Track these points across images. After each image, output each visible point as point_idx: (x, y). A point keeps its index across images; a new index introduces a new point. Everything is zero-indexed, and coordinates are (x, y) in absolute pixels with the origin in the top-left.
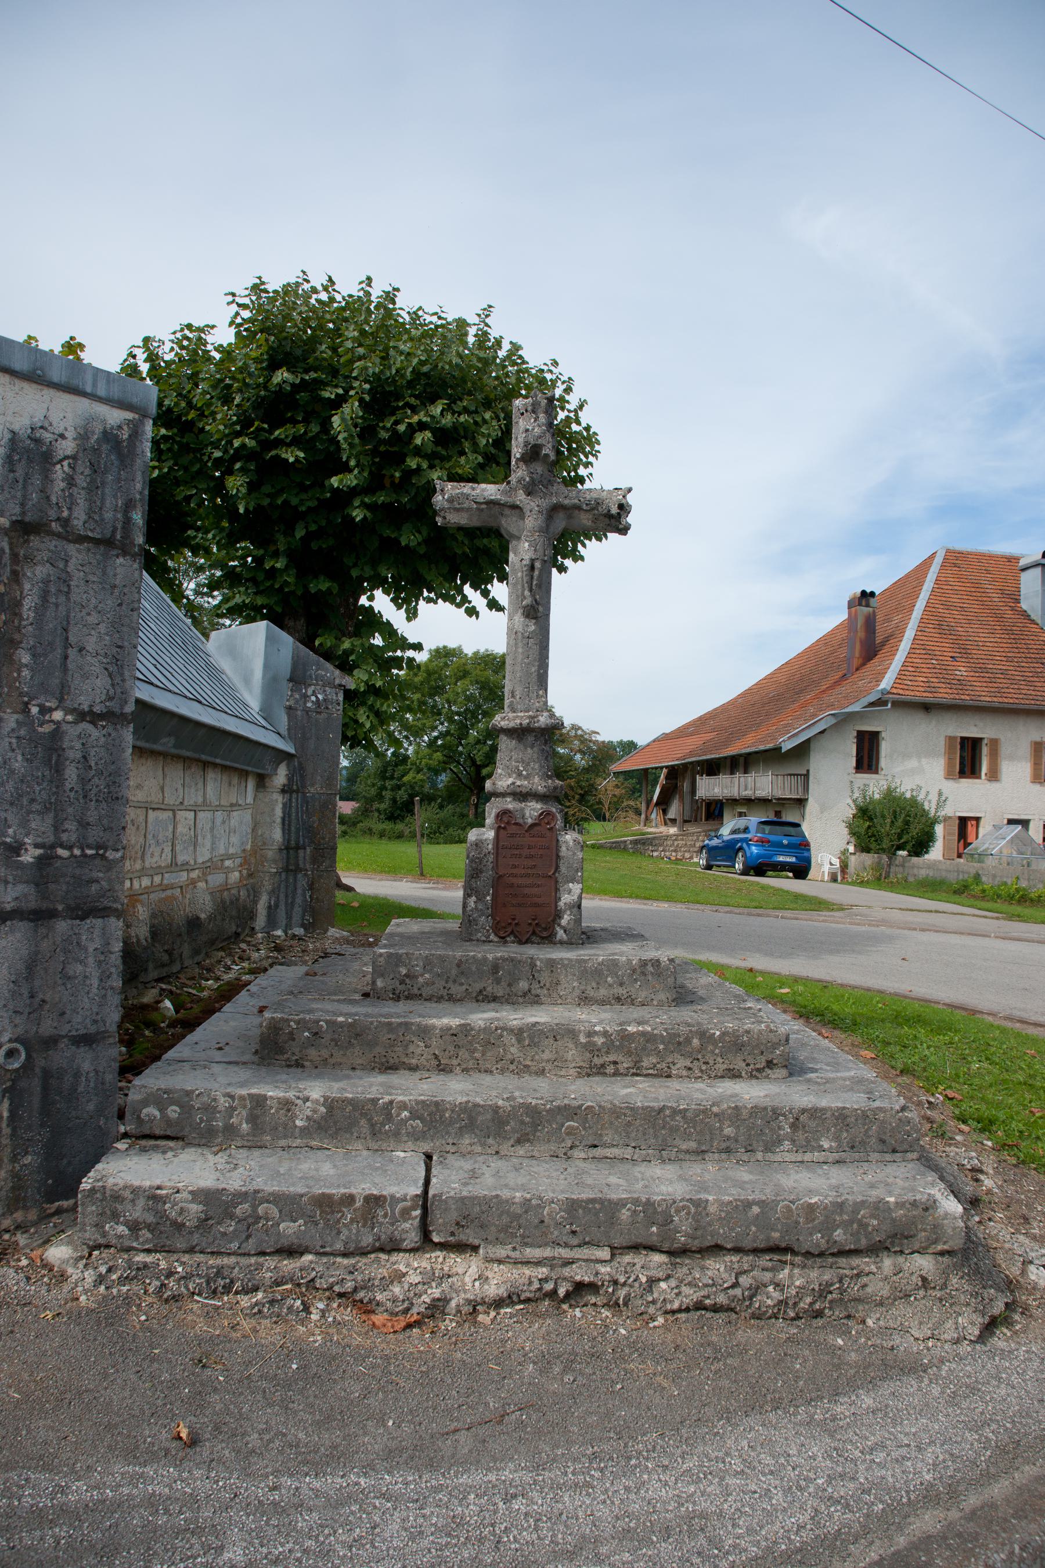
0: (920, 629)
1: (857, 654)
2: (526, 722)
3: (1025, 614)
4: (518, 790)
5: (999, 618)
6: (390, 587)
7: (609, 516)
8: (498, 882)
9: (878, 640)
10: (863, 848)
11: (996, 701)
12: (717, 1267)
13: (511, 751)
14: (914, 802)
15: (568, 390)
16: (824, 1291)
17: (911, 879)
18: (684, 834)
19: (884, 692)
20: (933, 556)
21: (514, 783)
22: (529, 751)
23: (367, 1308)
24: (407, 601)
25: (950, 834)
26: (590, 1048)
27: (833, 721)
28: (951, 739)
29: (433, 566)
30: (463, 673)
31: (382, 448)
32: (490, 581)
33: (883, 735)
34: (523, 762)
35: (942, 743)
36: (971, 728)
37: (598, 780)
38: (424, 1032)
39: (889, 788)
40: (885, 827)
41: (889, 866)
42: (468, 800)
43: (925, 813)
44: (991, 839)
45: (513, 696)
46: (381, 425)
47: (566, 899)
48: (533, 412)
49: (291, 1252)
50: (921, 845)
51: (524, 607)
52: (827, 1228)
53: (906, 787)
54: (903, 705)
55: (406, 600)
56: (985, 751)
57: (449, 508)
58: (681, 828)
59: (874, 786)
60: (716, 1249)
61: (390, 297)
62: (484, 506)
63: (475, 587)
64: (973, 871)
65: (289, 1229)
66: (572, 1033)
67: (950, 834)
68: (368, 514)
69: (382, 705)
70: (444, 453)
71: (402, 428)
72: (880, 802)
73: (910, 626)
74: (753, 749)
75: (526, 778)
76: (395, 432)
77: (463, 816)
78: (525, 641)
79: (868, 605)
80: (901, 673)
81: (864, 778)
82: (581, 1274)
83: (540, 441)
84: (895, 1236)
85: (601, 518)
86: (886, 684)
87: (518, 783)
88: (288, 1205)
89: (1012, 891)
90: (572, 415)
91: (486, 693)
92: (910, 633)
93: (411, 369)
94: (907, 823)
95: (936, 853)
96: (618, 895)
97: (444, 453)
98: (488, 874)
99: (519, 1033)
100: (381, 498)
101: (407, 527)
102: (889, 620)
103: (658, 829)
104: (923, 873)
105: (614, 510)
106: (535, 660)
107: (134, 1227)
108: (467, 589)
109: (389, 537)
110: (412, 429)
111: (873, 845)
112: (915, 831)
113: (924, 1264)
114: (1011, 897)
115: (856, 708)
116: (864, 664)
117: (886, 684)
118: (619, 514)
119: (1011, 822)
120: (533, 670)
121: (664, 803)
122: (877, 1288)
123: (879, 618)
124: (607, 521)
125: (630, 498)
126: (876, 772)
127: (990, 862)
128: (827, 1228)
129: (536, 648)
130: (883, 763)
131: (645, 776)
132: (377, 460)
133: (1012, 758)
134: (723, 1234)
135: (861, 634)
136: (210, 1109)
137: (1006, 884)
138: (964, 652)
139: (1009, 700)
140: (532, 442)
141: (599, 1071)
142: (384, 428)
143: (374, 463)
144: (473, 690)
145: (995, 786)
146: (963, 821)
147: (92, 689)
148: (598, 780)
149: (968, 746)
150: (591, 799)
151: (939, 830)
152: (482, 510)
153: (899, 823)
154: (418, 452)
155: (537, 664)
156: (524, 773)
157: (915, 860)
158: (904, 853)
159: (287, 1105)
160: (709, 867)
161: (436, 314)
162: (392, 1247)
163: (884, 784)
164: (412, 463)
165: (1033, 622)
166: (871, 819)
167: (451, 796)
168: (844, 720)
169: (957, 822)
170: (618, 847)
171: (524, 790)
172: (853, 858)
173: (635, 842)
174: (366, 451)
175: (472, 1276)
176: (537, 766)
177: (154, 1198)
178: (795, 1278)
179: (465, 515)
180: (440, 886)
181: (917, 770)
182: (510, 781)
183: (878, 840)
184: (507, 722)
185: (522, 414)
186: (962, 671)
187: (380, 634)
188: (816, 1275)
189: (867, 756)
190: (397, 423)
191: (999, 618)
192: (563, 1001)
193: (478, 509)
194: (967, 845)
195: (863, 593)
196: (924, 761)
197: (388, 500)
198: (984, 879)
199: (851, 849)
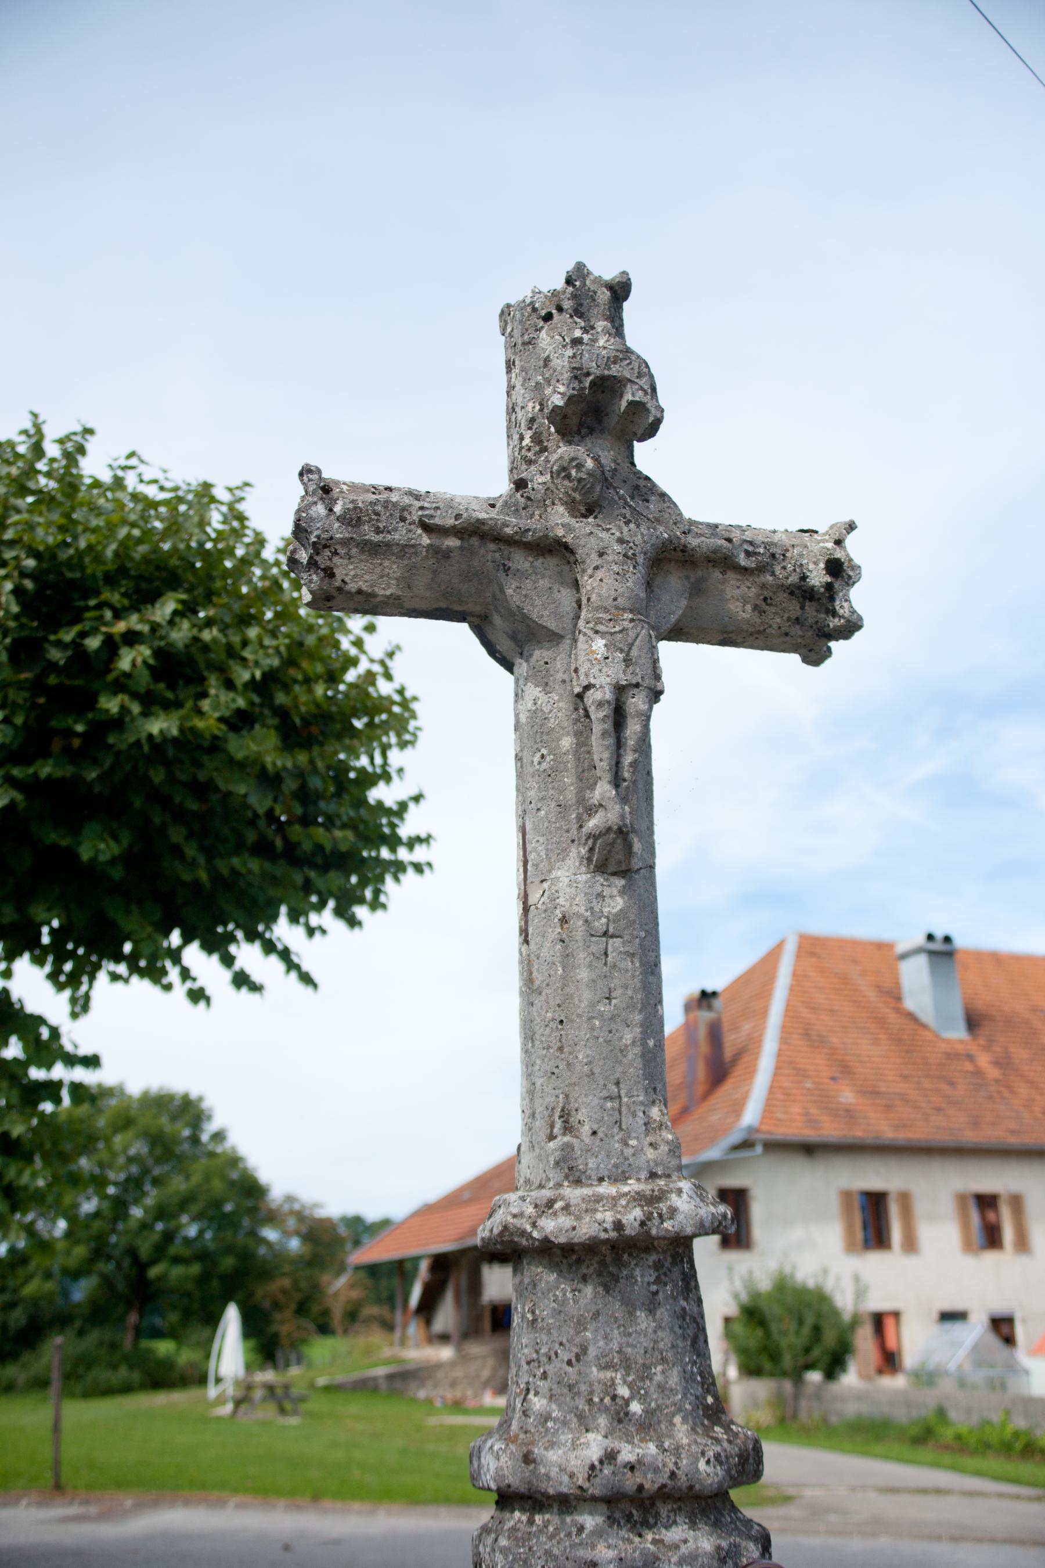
0: (785, 1038)
2: (633, 1216)
3: (911, 1017)
4: (630, 1482)
5: (881, 1022)
6: (45, 950)
7: (803, 592)
11: (901, 1136)
13: (581, 1325)
18: (463, 1358)
19: (750, 1130)
21: (610, 1456)
22: (643, 1321)
24: (73, 980)
28: (846, 1196)
29: (134, 908)
30: (125, 1121)
31: (52, 680)
32: (231, 938)
34: (627, 1364)
35: (834, 1204)
36: (874, 1176)
37: (325, 1278)
40: (790, 1339)
42: (122, 1319)
43: (835, 1313)
45: (568, 1129)
46: (52, 638)
48: (578, 312)
50: (834, 1365)
51: (594, 837)
53: (805, 1272)
54: (777, 1147)
55: (73, 980)
56: (894, 1211)
57: (346, 542)
58: (458, 1349)
61: (74, 450)
62: (452, 542)
63: (209, 947)
68: (19, 797)
69: (20, 1173)
70: (170, 695)
71: (93, 643)
72: (770, 1296)
75: (647, 1426)
77: (114, 1346)
78: (597, 945)
79: (710, 1008)
83: (614, 370)
85: (782, 596)
86: (751, 1115)
87: (627, 1454)
90: (377, 668)
91: (158, 1151)
93: (113, 547)
94: (817, 1329)
96: (413, 1498)
97: (170, 695)
100: (46, 769)
101: (91, 829)
102: (736, 1029)
103: (419, 1352)
105: (818, 577)
106: (631, 1006)
108: (194, 955)
109: (55, 846)
110: (111, 647)
111: (768, 1366)
112: (830, 1338)
115: (714, 1153)
117: (751, 1115)
118: (829, 587)
120: (628, 1037)
121: (427, 1308)
123: (726, 1026)
124: (793, 608)
125: (855, 548)
129: (632, 966)
131: (401, 1270)
132: (41, 700)
135: (704, 1048)
138: (845, 1069)
139: (919, 1134)
140: (596, 372)
142: (59, 644)
143: (34, 706)
144: (139, 1148)
145: (1023, 1260)
148: (325, 1278)
150: (315, 1309)
152: (446, 554)
153: (806, 1330)
154: (121, 685)
155: (638, 1018)
156: (636, 1407)
161: (156, 481)
164: (111, 704)
165: (924, 1026)
167: (98, 1314)
170: (365, 1387)
171: (651, 1482)
173: (391, 1377)
174: (19, 682)
176: (674, 1379)
179: (393, 568)
180: (93, 1510)
182: (594, 1446)
184: (565, 1221)
185: (548, 317)
186: (847, 1096)
187: (20, 1038)
190: (83, 635)
191: (881, 1022)
193: (435, 551)
195: (704, 994)
197: (59, 773)
198: (952, 1415)
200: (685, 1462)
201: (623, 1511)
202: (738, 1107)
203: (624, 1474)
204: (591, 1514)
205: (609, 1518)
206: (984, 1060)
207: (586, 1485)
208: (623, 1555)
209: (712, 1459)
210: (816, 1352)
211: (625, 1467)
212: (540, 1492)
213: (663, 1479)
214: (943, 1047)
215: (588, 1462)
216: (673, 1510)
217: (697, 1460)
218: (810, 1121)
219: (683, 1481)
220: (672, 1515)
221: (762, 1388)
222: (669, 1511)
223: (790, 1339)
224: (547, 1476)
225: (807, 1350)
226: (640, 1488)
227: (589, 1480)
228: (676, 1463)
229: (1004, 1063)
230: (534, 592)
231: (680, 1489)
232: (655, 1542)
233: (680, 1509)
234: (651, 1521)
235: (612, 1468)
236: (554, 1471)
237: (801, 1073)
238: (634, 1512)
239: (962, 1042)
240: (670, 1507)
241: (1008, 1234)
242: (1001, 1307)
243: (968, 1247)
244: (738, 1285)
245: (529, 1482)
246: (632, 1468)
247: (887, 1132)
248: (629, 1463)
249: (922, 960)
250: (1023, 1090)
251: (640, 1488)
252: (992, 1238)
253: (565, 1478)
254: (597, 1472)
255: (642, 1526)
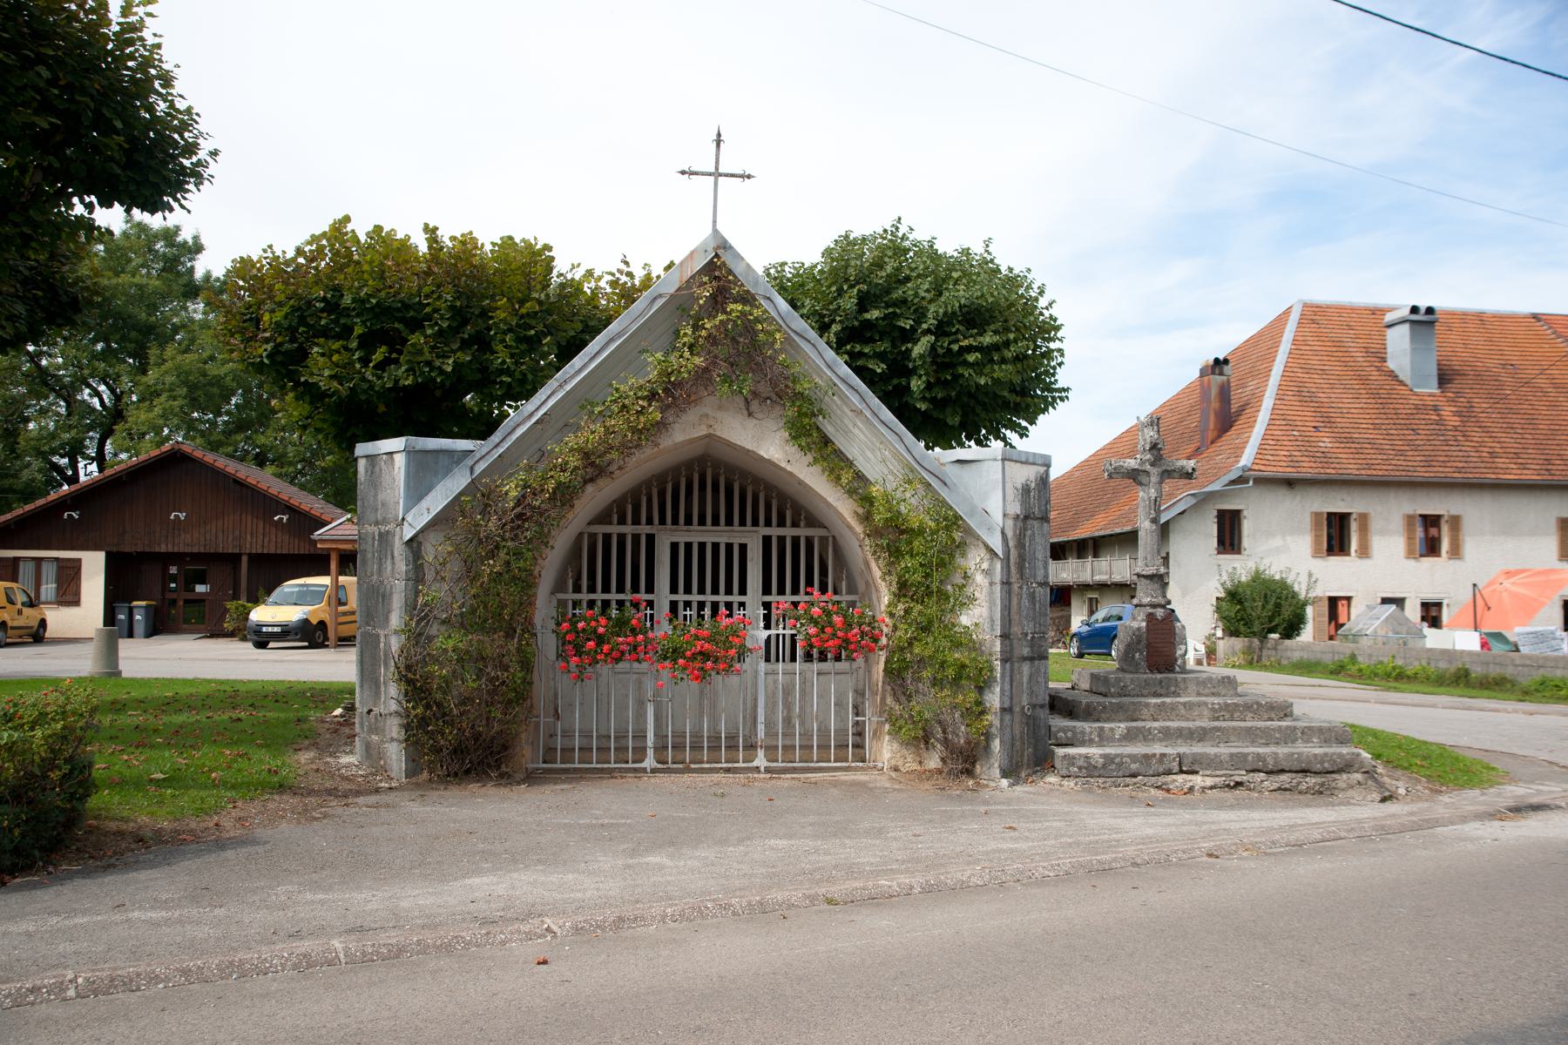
0: (1279, 398)
1: (1212, 426)
3: (1392, 375)
5: (1364, 380)
8: (1148, 646)
9: (1234, 407)
10: (1232, 632)
12: (1285, 777)
14: (1283, 585)
15: (1041, 293)
16: (1322, 784)
17: (1284, 662)
19: (1245, 469)
20: (1287, 312)
23: (1168, 791)
25: (1320, 615)
26: (1213, 710)
27: (1193, 501)
33: (1245, 513)
35: (1307, 521)
38: (1147, 705)
39: (1257, 571)
40: (1257, 610)
41: (1261, 649)
43: (1295, 595)
44: (1364, 618)
47: (1179, 652)
49: (1134, 776)
50: (1292, 628)
52: (1322, 762)
53: (1275, 568)
54: (1264, 482)
56: (1354, 526)
59: (1241, 567)
60: (1282, 771)
64: (1348, 652)
65: (1134, 767)
66: (1206, 704)
67: (1320, 615)
71: (955, 347)
72: (1248, 585)
73: (1267, 394)
74: (1108, 532)
76: (949, 350)
79: (1221, 374)
80: (1262, 447)
81: (1229, 561)
82: (1238, 779)
84: (1346, 767)
86: (1246, 459)
88: (1134, 758)
89: (1389, 669)
92: (1268, 403)
94: (1278, 606)
95: (1307, 635)
98: (1144, 642)
99: (1184, 704)
101: (949, 410)
102: (1243, 386)
104: (1296, 656)
107: (1080, 768)
111: (1242, 629)
112: (1287, 613)
113: (1358, 776)
114: (1388, 675)
115: (1216, 486)
116: (1219, 437)
117: (1246, 459)
119: (1385, 601)
122: (1341, 784)
126: (1239, 552)
127: (1365, 642)
128: (1322, 762)
130: (1246, 542)
133: (1383, 532)
134: (1286, 766)
135: (1215, 405)
136: (1083, 733)
137: (1381, 663)
141: (1217, 719)
145: (1365, 563)
146: (1333, 602)
147: (1040, 578)
149: (1336, 522)
151: (1309, 610)
153: (1270, 606)
157: (1287, 642)
158: (1275, 636)
159: (1112, 730)
160: (1080, 655)
162: (1169, 773)
163: (1251, 565)
165: (1402, 383)
166: (1240, 602)
168: (1204, 499)
169: (1128, 528)
172: (1221, 644)
175: (1198, 780)
177: (1087, 757)
178: (1311, 780)
181: (1282, 549)
183: (1248, 624)
186: (1326, 443)
188: (1319, 780)
189: (1229, 536)
191: (1364, 380)
192: (1189, 695)
194: (1339, 626)
195: (1217, 361)
196: (1289, 539)
198: (1360, 659)
199: (1219, 633)
202: (1238, 452)
206: (1447, 411)
210: (1277, 621)
214: (1414, 400)
218: (1294, 463)
221: (1238, 643)
223: (1257, 610)
225: (1271, 619)
229: (1465, 414)
230: (1143, 479)
237: (1290, 425)
239: (1431, 395)
241: (1445, 545)
242: (1431, 596)
243: (1410, 554)
244: (1225, 577)
247: (1352, 469)
249: (1406, 328)
250: (1477, 436)
252: (1432, 548)
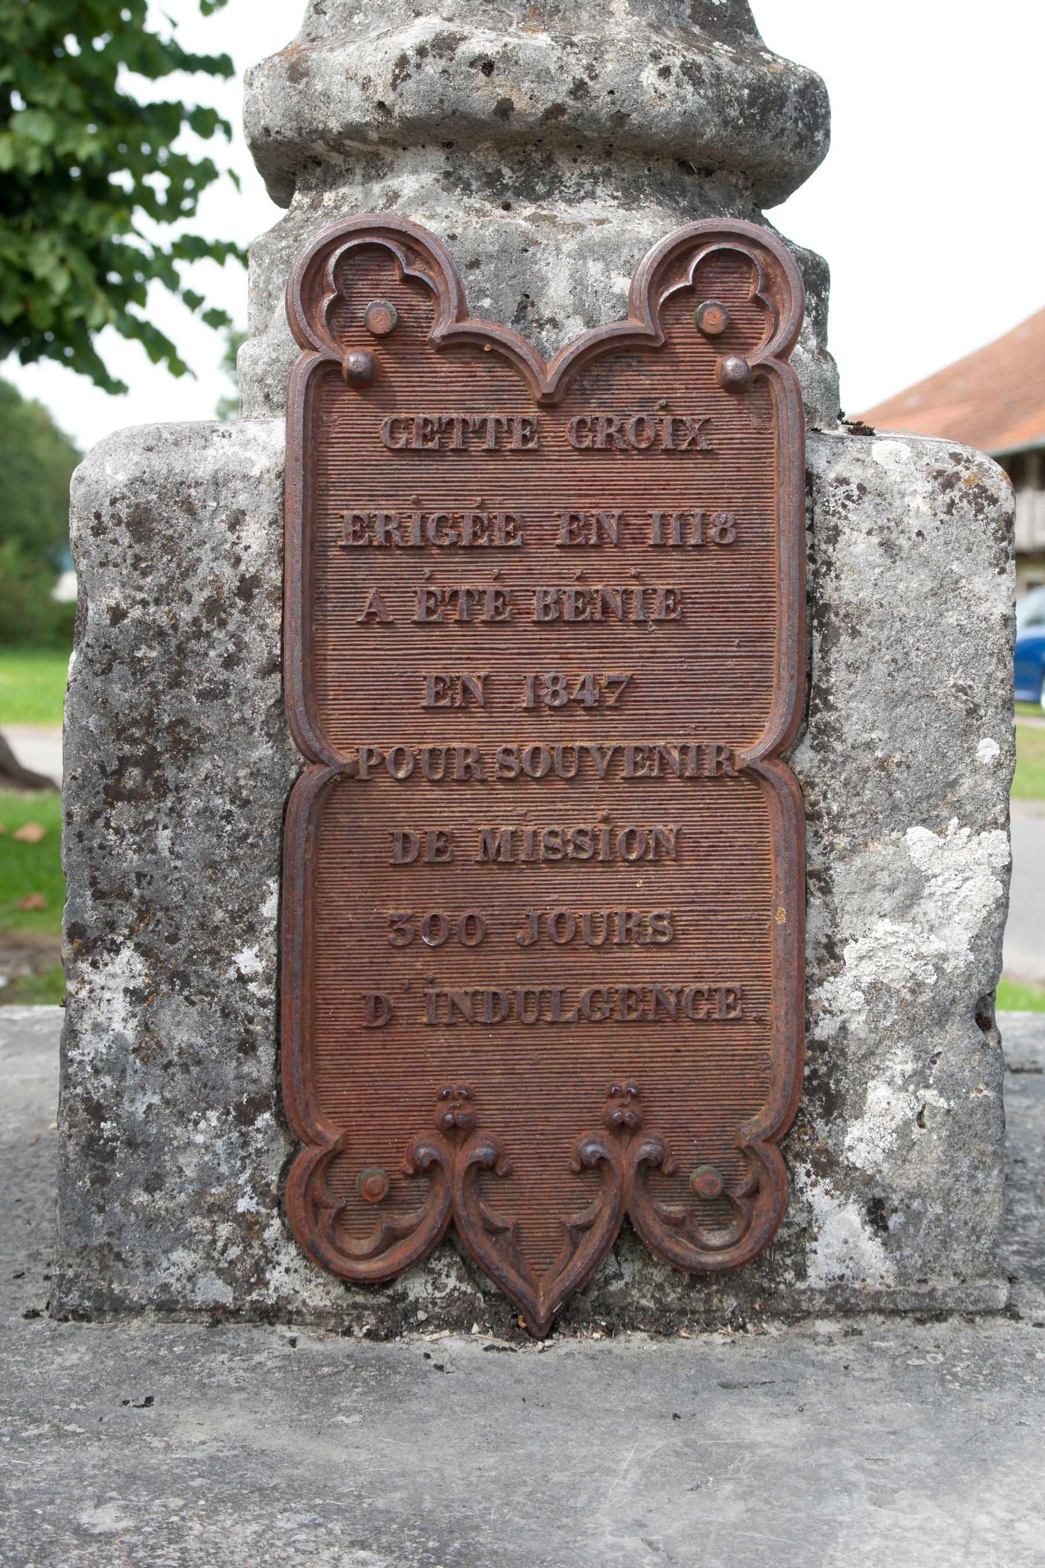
4: (481, 96)
171: (529, 100)
200: (610, 66)
201: (480, 167)
203: (469, 77)
204: (415, 171)
205: (447, 175)
207: (390, 98)
208: (458, 231)
209: (675, 70)
211: (472, 64)
212: (323, 134)
213: (558, 93)
215: (396, 54)
216: (592, 175)
217: (640, 66)
219: (602, 104)
220: (588, 186)
222: (582, 176)
224: (326, 95)
226: (505, 108)
227: (394, 86)
228: (590, 68)
231: (594, 119)
232: (533, 219)
233: (608, 173)
234: (541, 189)
235: (443, 63)
236: (337, 85)
238: (506, 171)
240: (586, 169)
245: (298, 114)
246: (488, 67)
248: (480, 57)
251: (505, 108)
253: (355, 93)
254: (411, 69)
255: (517, 194)
